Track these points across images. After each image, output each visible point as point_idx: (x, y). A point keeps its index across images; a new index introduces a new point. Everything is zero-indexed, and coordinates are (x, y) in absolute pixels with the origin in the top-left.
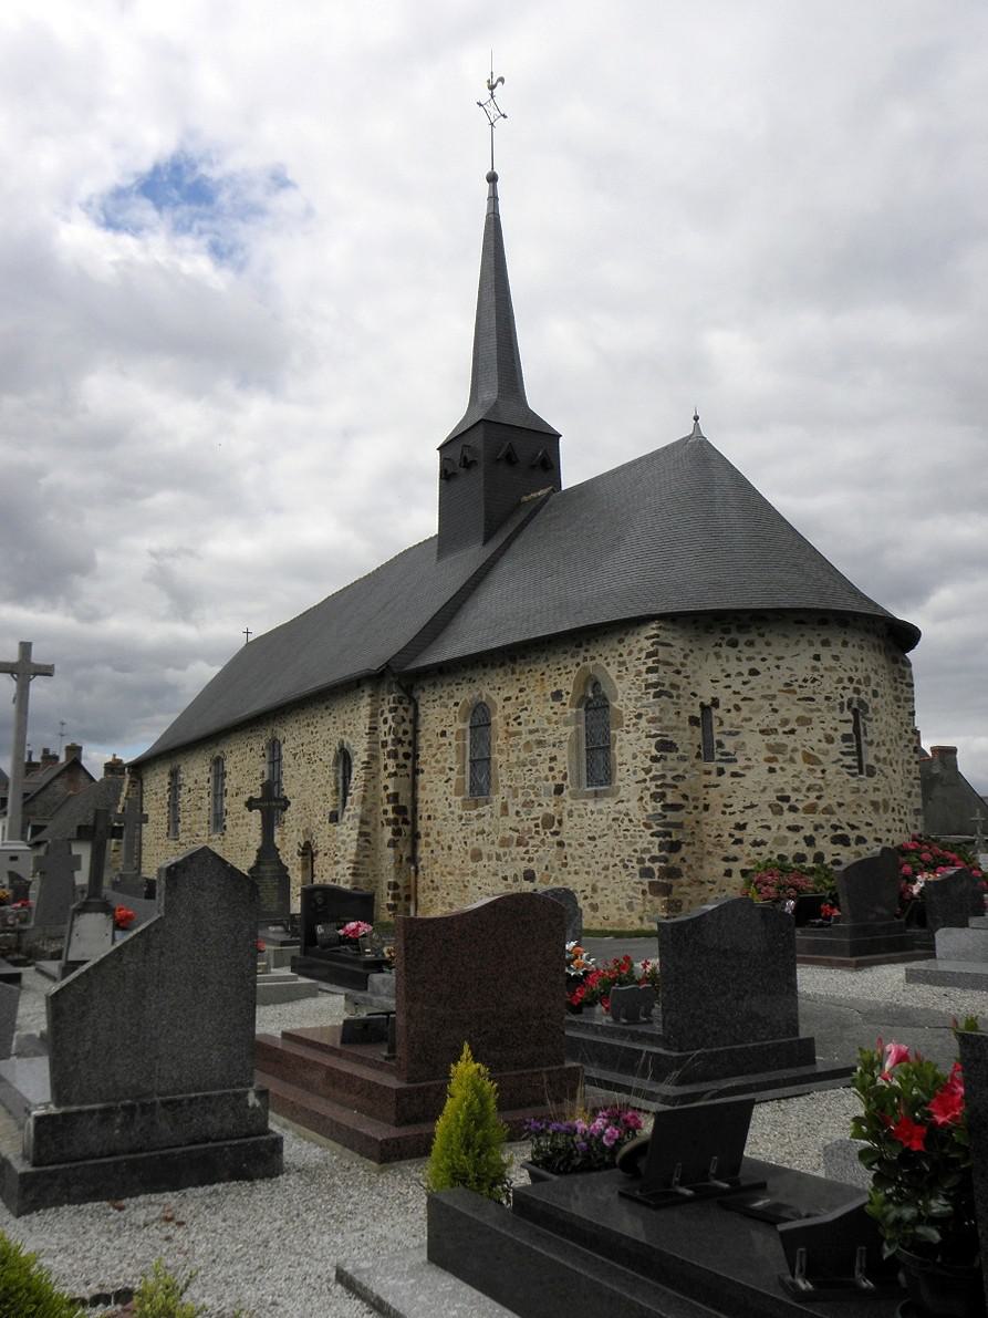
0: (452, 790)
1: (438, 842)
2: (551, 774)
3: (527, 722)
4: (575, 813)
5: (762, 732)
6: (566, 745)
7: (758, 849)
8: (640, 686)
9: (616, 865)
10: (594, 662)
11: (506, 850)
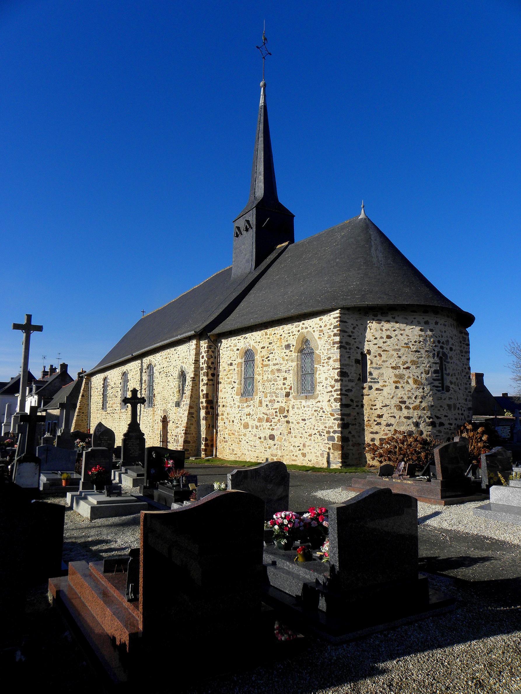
5: (392, 368)
6: (291, 372)
9: (315, 434)
10: (307, 330)
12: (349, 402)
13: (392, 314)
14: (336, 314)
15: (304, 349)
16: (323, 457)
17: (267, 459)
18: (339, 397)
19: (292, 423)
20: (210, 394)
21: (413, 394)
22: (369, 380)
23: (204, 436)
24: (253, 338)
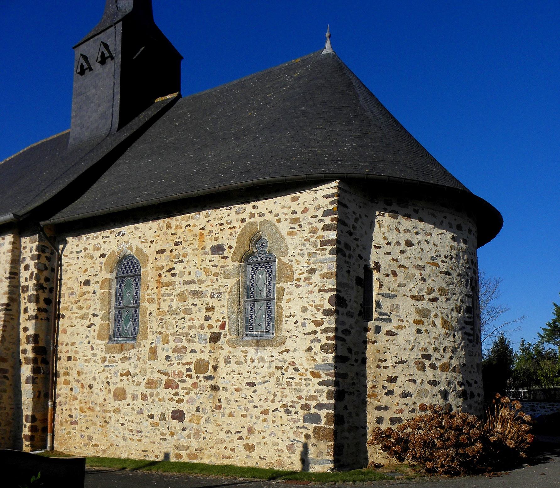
0: (96, 334)
1: (78, 381)
2: (206, 323)
3: (182, 274)
4: (233, 361)
5: (413, 297)
6: (225, 296)
7: (405, 400)
8: (315, 242)
9: (276, 410)
10: (262, 219)
11: (152, 391)
12: (346, 354)
13: (414, 205)
14: (332, 187)
15: (253, 254)
16: (293, 452)
17: (167, 455)
18: (333, 342)
19: (225, 389)
20: (42, 336)
21: (441, 344)
22: (375, 315)
23: (30, 413)
24: (138, 233)
